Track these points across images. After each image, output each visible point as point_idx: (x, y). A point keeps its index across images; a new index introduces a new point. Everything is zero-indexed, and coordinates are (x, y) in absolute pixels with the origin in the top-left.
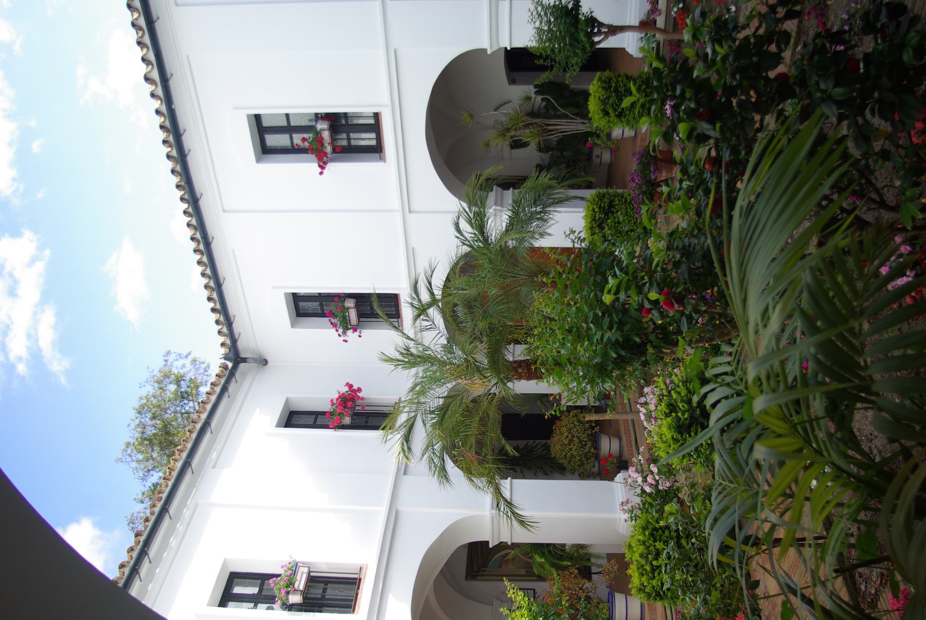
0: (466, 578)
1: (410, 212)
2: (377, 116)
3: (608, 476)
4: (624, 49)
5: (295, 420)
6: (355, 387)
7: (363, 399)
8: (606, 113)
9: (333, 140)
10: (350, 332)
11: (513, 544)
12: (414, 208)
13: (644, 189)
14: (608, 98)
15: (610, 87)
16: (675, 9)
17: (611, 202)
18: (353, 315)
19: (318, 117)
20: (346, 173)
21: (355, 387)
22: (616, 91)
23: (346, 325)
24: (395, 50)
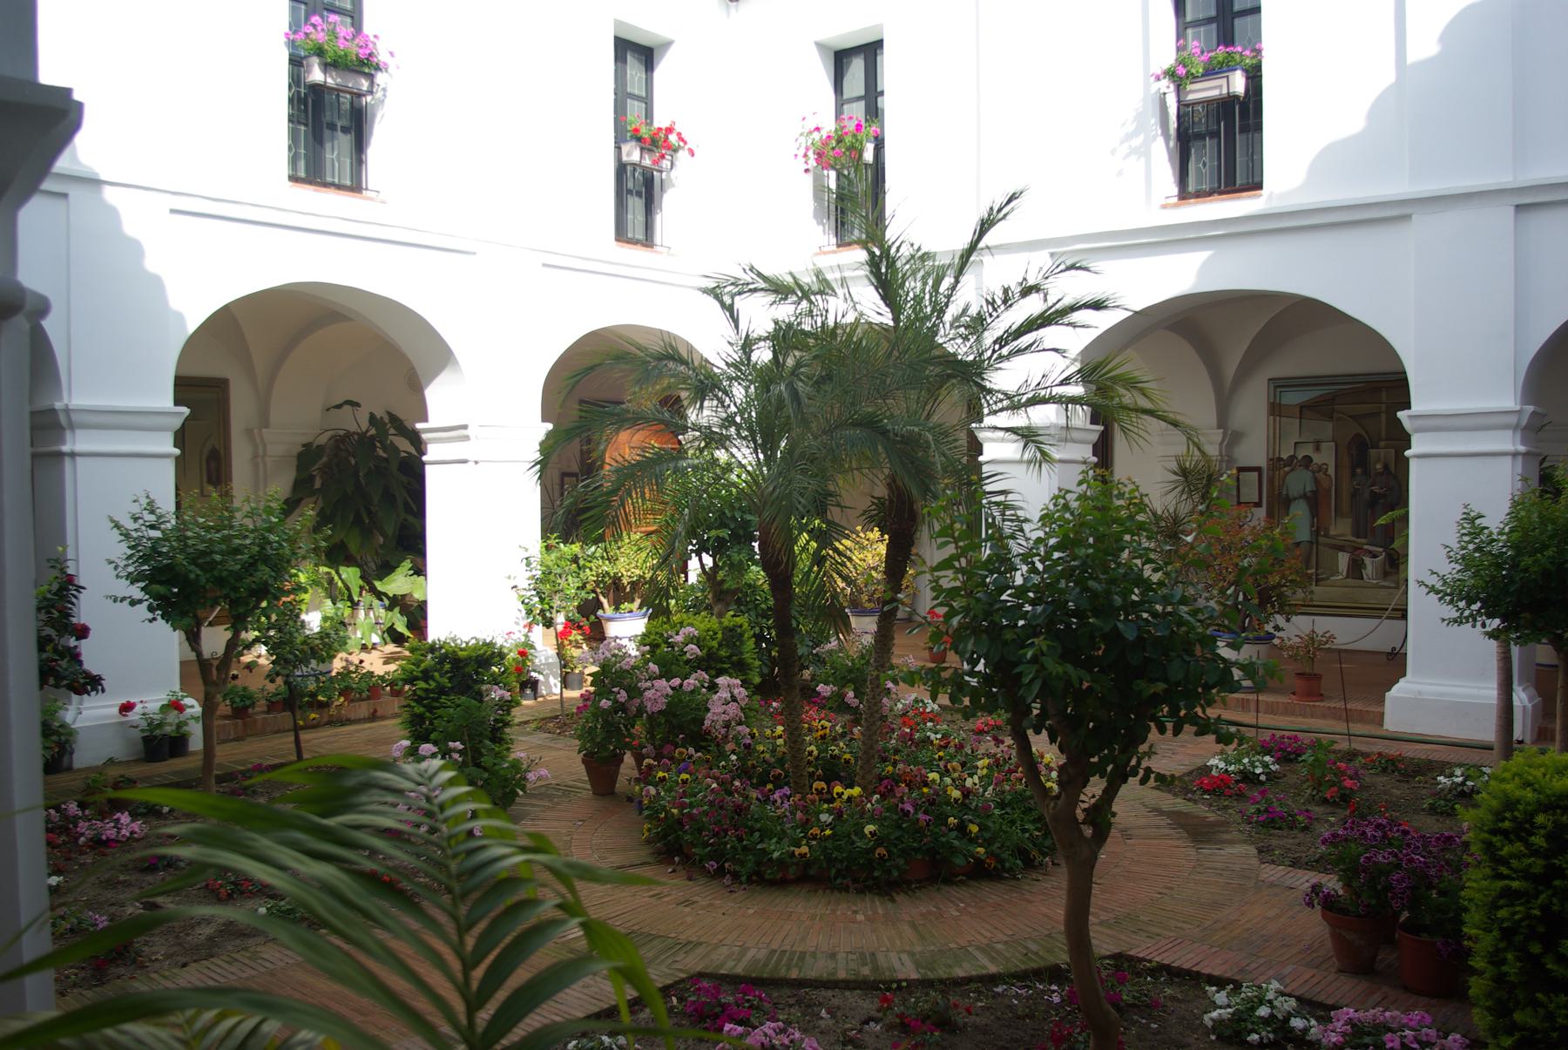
19: (1254, 77)
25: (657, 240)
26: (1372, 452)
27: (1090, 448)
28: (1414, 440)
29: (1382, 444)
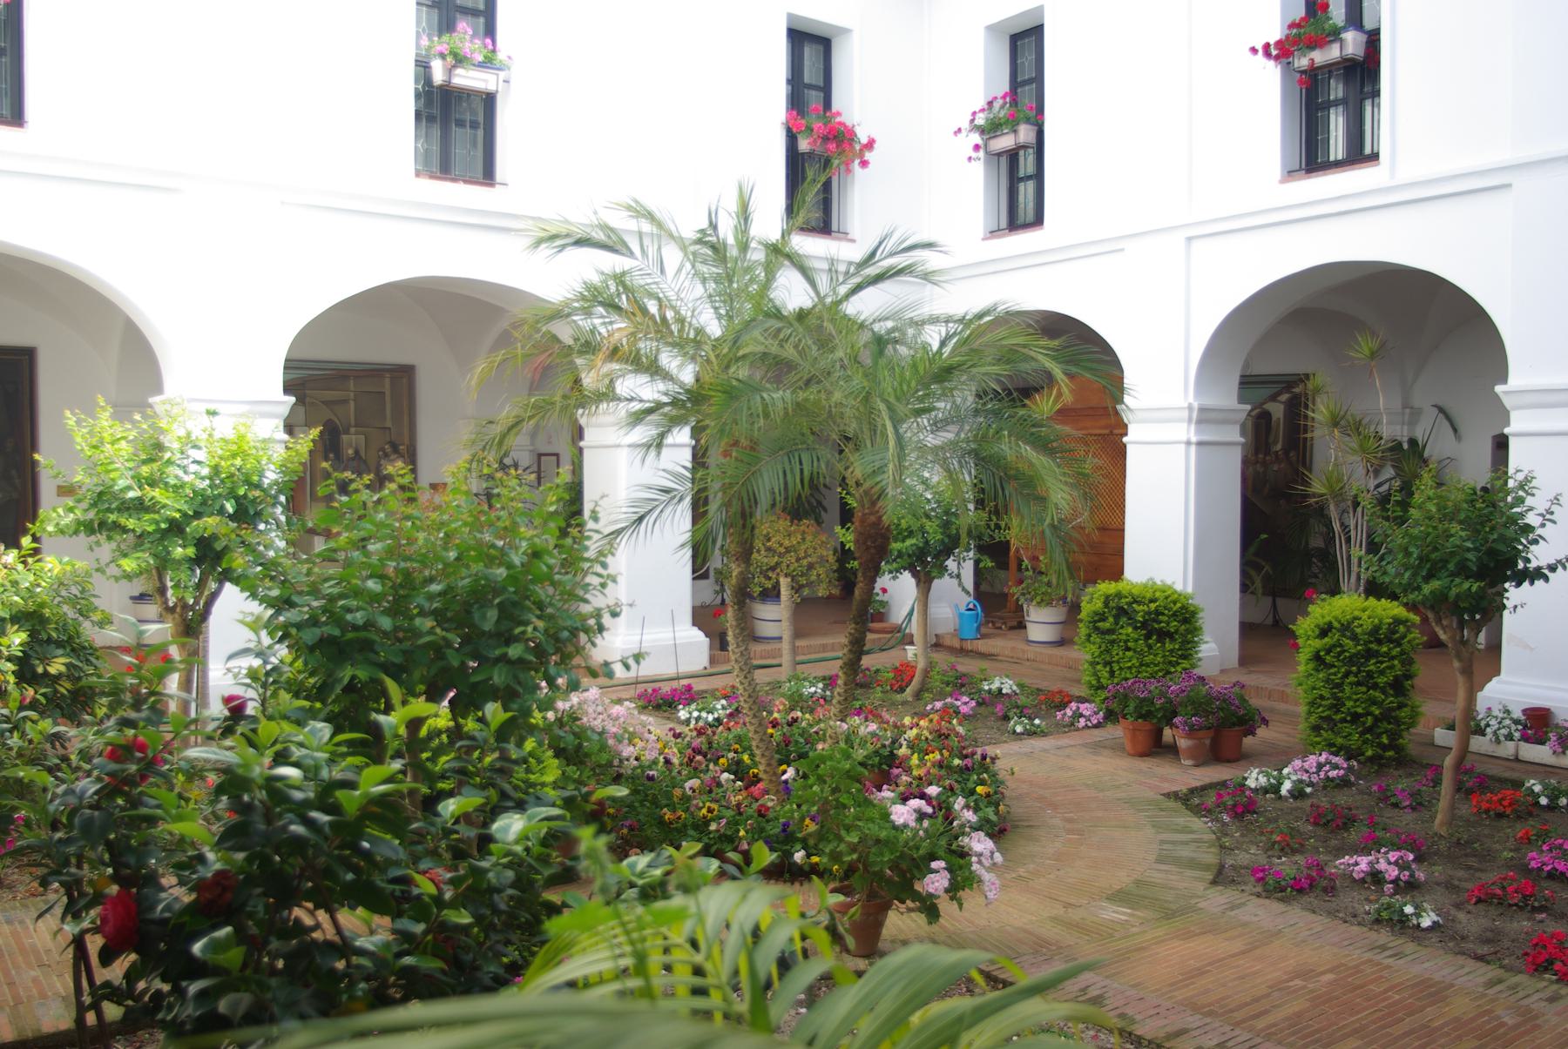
0: (404, 375)
1: (1189, 239)
2: (1374, 157)
3: (703, 617)
4: (1498, 673)
5: (809, 52)
6: (868, 156)
7: (849, 171)
8: (1324, 631)
9: (1329, 68)
10: (976, 138)
11: (581, 450)
12: (1196, 244)
13: (1158, 703)
14: (1354, 637)
15: (1380, 642)
16: (1537, 788)
17: (1171, 636)
18: (1005, 142)
19: (1373, 39)
20: (1262, 99)
21: (868, 156)
22: (1369, 654)
23: (991, 129)
24: (1509, 186)
25: (834, 227)
26: (345, 437)
27: (1237, 428)
28: (1514, 416)
29: (353, 430)
